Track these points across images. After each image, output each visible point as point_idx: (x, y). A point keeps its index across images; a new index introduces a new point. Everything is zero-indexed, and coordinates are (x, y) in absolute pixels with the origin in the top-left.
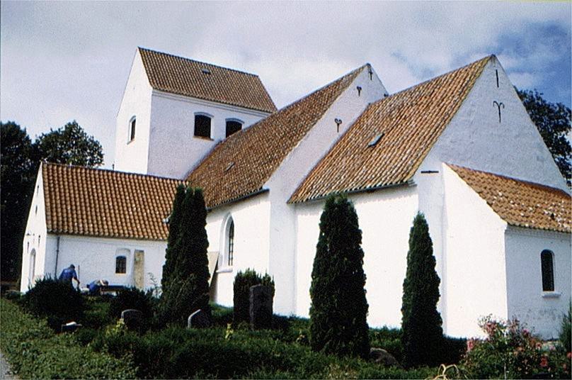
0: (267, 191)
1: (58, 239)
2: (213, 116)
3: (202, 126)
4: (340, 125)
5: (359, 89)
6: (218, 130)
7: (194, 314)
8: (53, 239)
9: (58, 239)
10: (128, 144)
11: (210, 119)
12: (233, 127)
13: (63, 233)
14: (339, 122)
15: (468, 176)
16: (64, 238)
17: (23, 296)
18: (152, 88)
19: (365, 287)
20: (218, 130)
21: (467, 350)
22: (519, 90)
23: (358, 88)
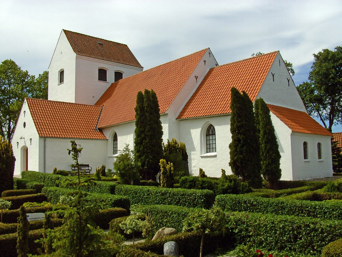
0: (167, 114)
1: (45, 140)
2: (124, 72)
3: (102, 74)
4: (197, 79)
5: (205, 61)
6: (111, 77)
7: (94, 181)
8: (43, 140)
9: (45, 140)
10: (58, 85)
11: (106, 71)
12: (118, 75)
13: (47, 137)
14: (196, 78)
15: (137, 64)
16: (48, 140)
17: (192, 177)
18: (76, 54)
19: (280, 168)
20: (111, 77)
21: (205, 209)
22: (284, 60)
23: (204, 61)
